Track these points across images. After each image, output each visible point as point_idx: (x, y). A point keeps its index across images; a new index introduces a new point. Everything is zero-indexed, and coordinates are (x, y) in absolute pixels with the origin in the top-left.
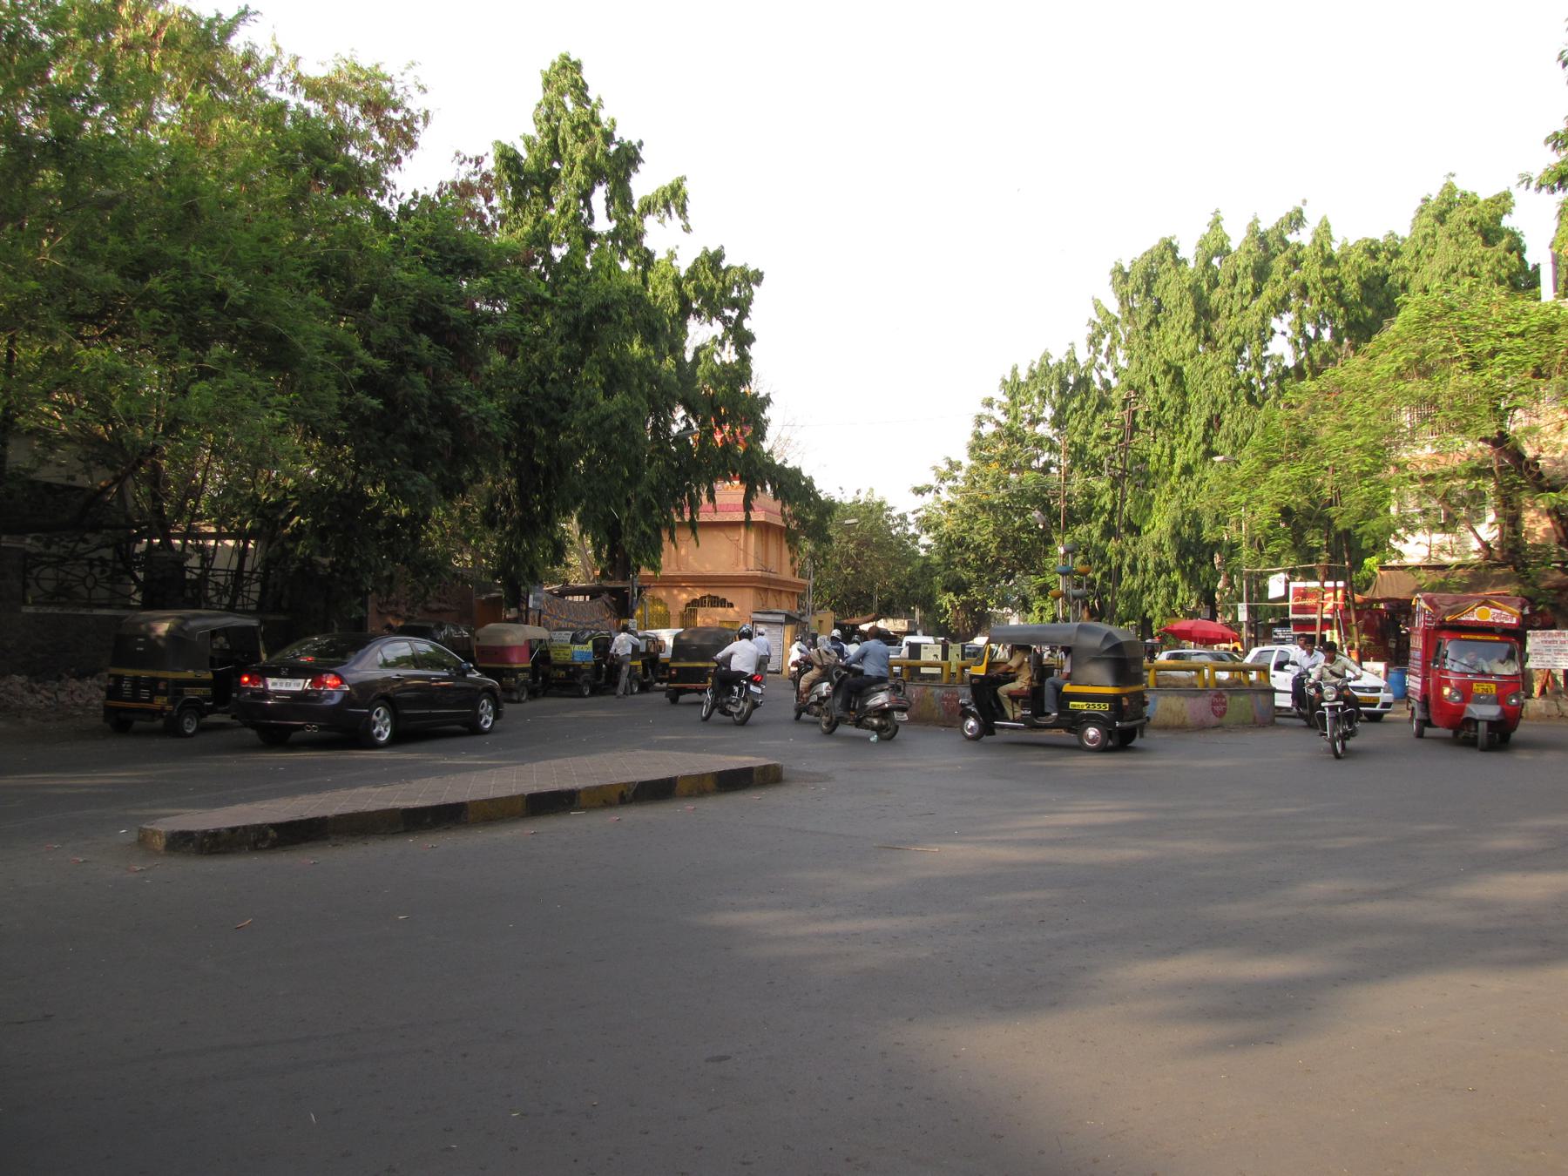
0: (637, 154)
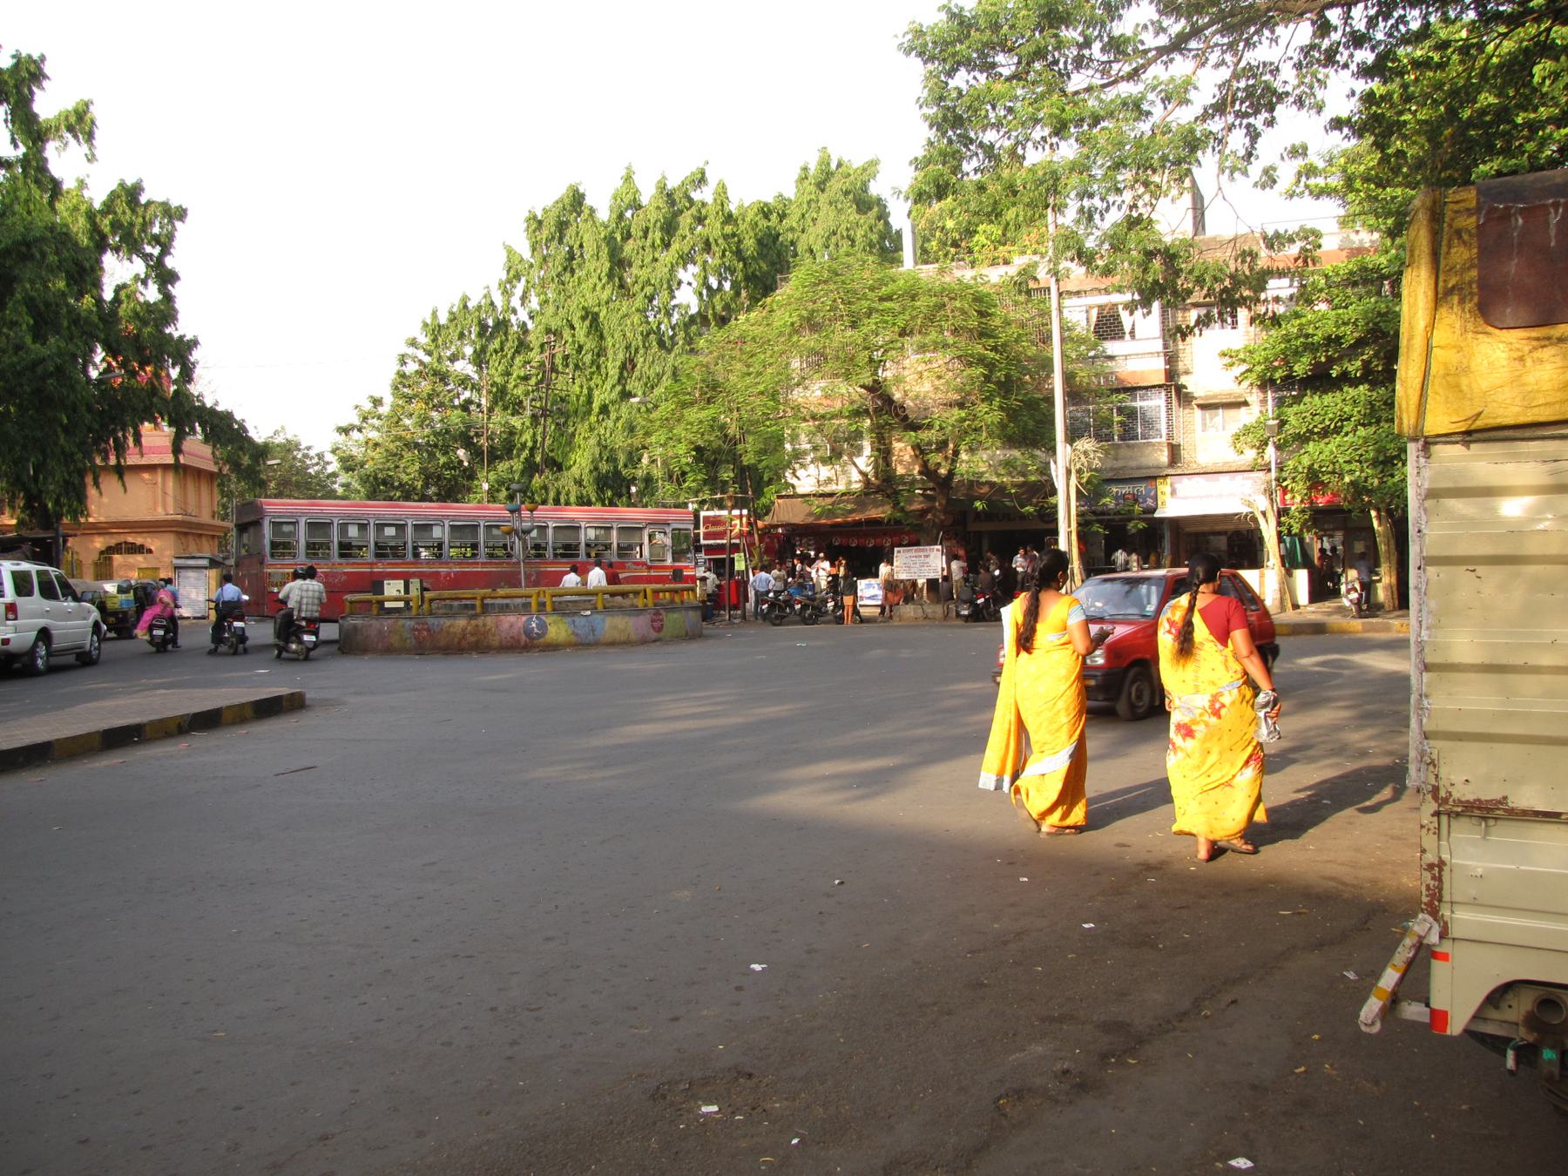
0: (40, 69)
